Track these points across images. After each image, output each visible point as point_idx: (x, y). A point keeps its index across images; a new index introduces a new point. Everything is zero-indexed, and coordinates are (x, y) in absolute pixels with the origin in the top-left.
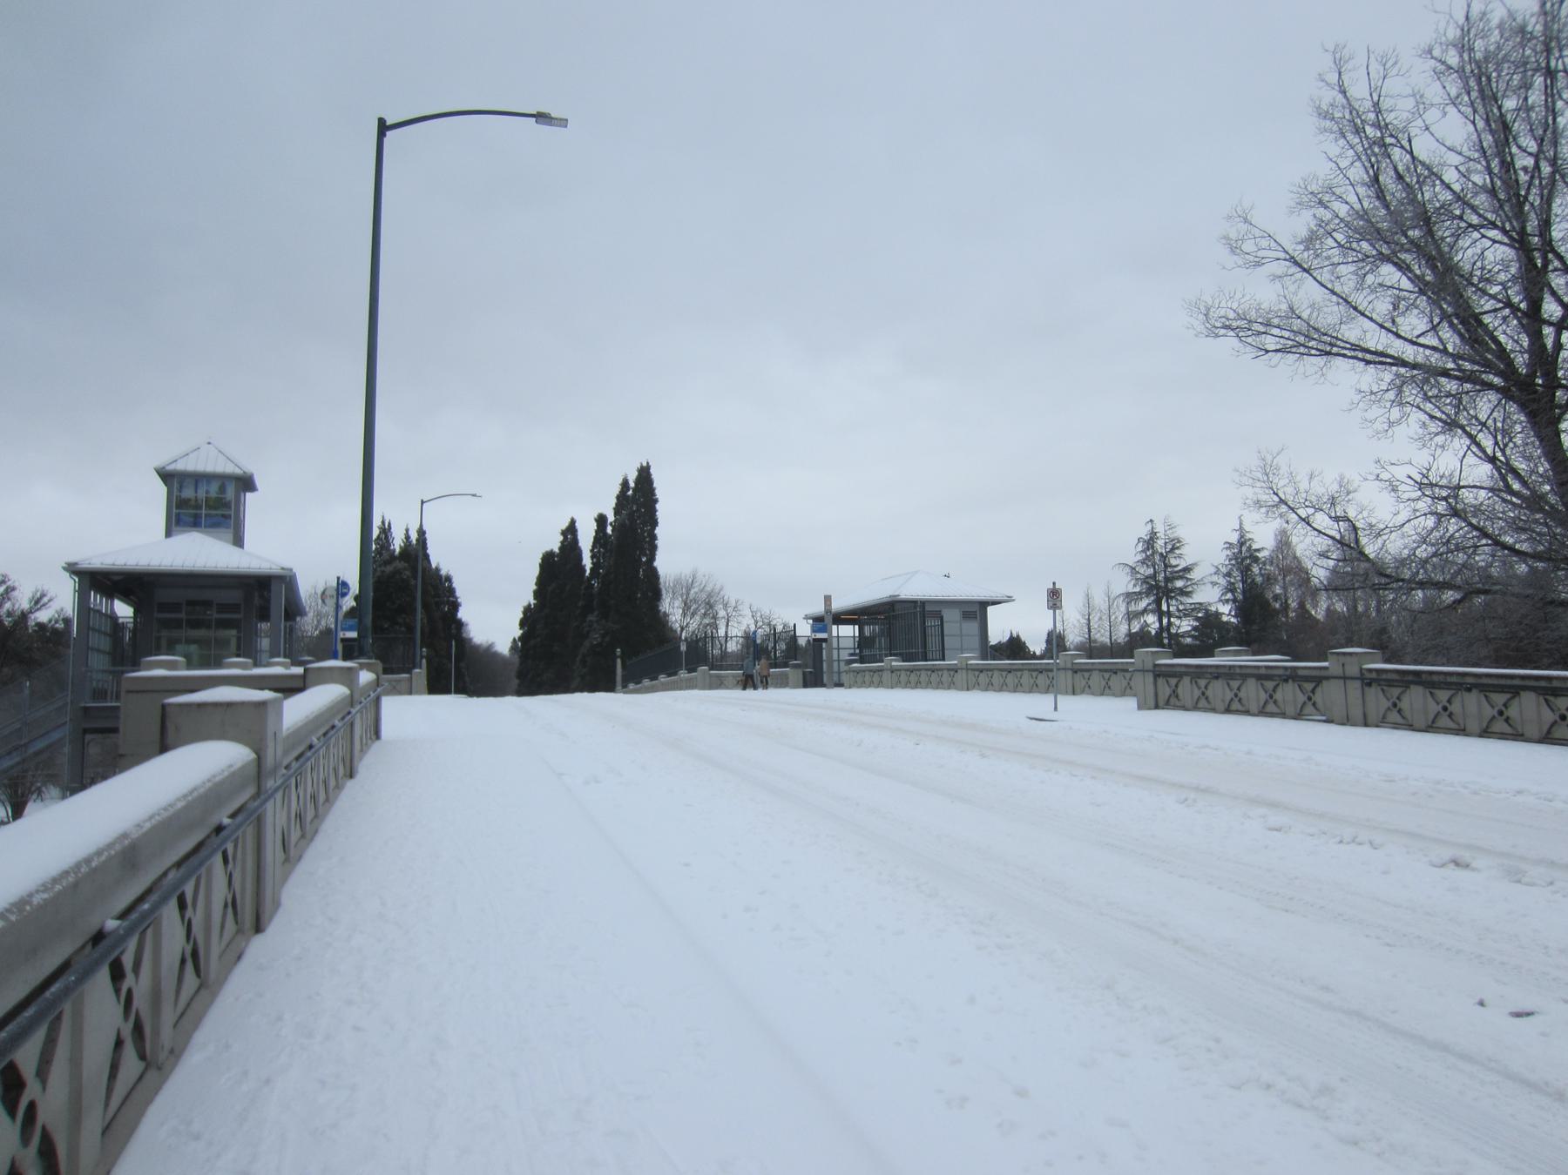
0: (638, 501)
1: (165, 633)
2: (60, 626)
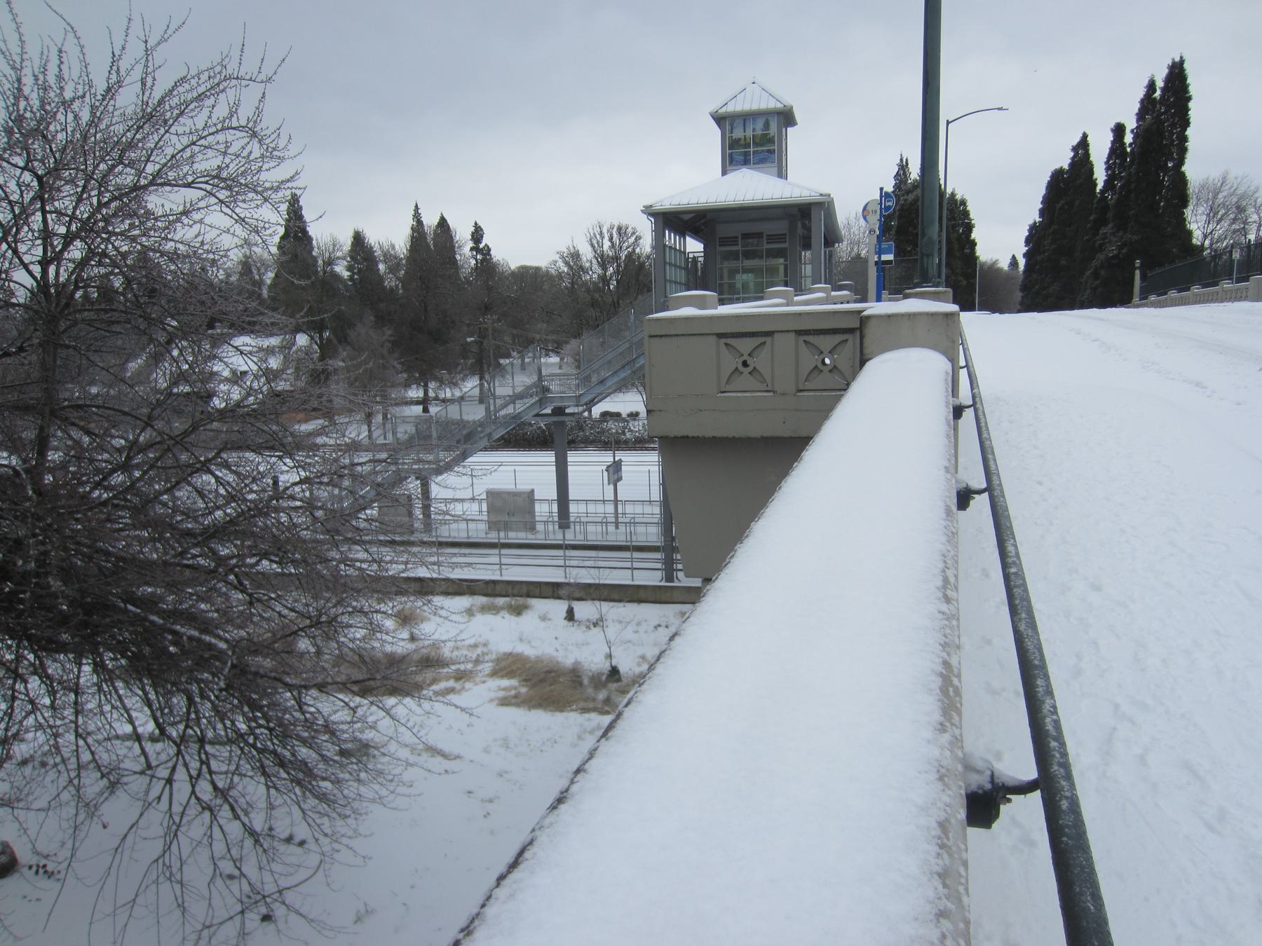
0: (1167, 107)
1: (726, 264)
2: (885, 294)
